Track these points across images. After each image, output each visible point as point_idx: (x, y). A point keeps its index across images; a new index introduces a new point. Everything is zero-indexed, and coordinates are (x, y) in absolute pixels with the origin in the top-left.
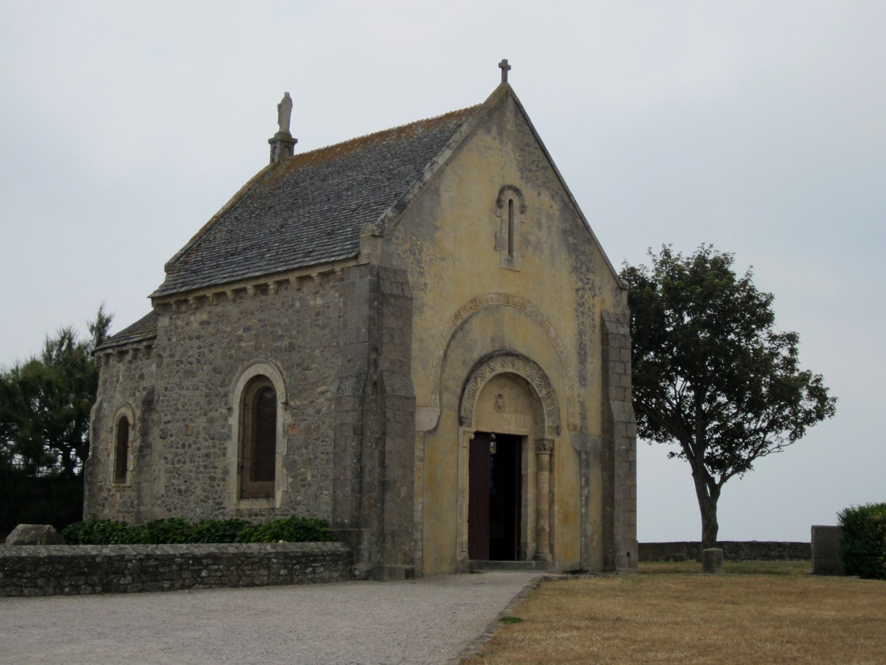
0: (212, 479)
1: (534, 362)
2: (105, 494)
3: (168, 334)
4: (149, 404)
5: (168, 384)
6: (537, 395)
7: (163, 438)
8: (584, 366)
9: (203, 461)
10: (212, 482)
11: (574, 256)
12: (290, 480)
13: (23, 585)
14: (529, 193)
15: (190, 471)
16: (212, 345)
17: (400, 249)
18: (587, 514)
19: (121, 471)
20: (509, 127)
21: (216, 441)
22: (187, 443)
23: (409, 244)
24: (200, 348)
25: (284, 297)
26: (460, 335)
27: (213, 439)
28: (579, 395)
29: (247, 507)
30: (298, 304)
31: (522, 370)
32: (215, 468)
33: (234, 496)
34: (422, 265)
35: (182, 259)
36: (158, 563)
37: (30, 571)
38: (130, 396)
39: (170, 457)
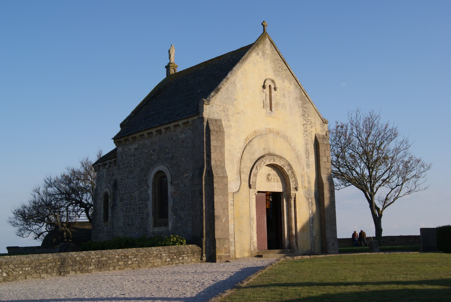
0: (142, 218)
1: (284, 158)
2: (100, 228)
3: (122, 154)
4: (115, 186)
5: (123, 177)
6: (286, 173)
7: (121, 201)
8: (308, 159)
9: (138, 211)
10: (142, 220)
11: (301, 109)
12: (175, 217)
13: (41, 272)
15: (133, 215)
16: (140, 159)
17: (218, 110)
18: (313, 227)
19: (106, 218)
20: (267, 52)
21: (143, 201)
22: (131, 203)
23: (222, 107)
24: (135, 160)
25: (169, 135)
26: (248, 147)
27: (142, 200)
28: (307, 172)
29: (158, 230)
30: (175, 138)
31: (278, 162)
32: (143, 213)
33: (152, 226)
34: (229, 117)
35: (127, 121)
36: (107, 259)
37: (44, 266)
38: (109, 183)
39: (124, 209)
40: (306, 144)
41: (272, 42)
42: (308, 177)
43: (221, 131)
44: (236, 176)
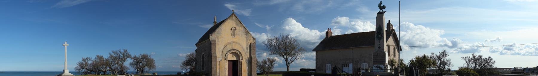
14: (237, 28)
26: (225, 47)
31: (236, 52)
40: (247, 46)
41: (235, 16)
43: (215, 44)
44: (220, 56)
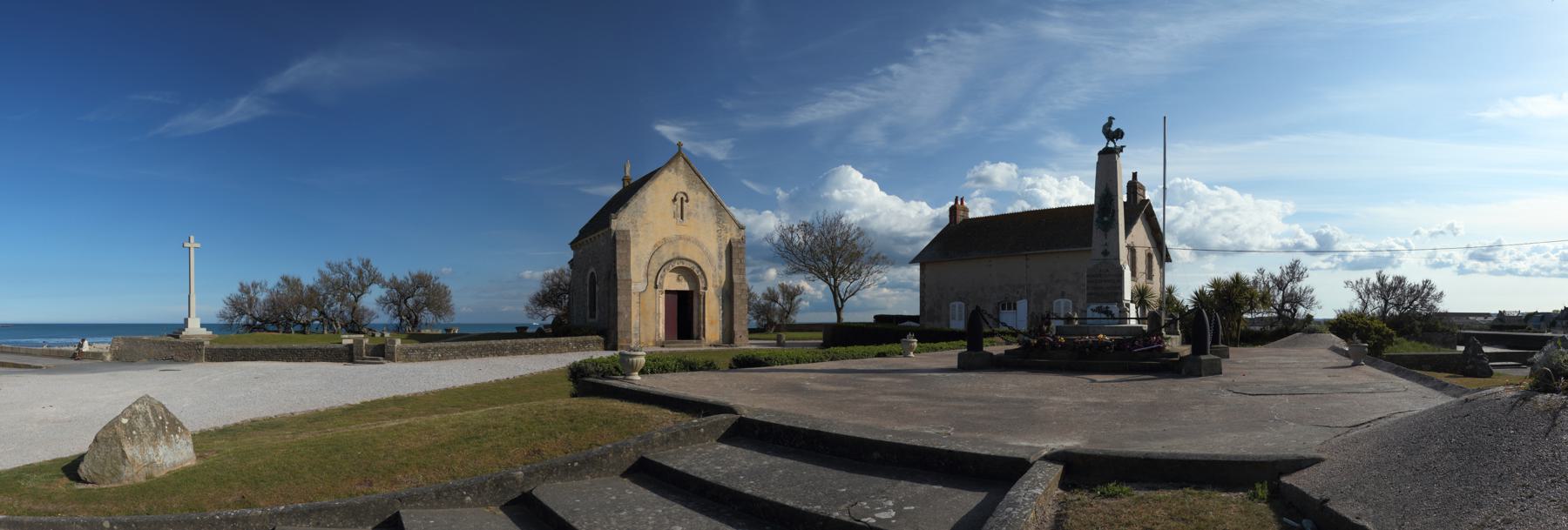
14: (691, 195)
31: (687, 265)
40: (720, 248)
41: (684, 159)
42: (720, 277)
43: (627, 243)
44: (643, 278)
